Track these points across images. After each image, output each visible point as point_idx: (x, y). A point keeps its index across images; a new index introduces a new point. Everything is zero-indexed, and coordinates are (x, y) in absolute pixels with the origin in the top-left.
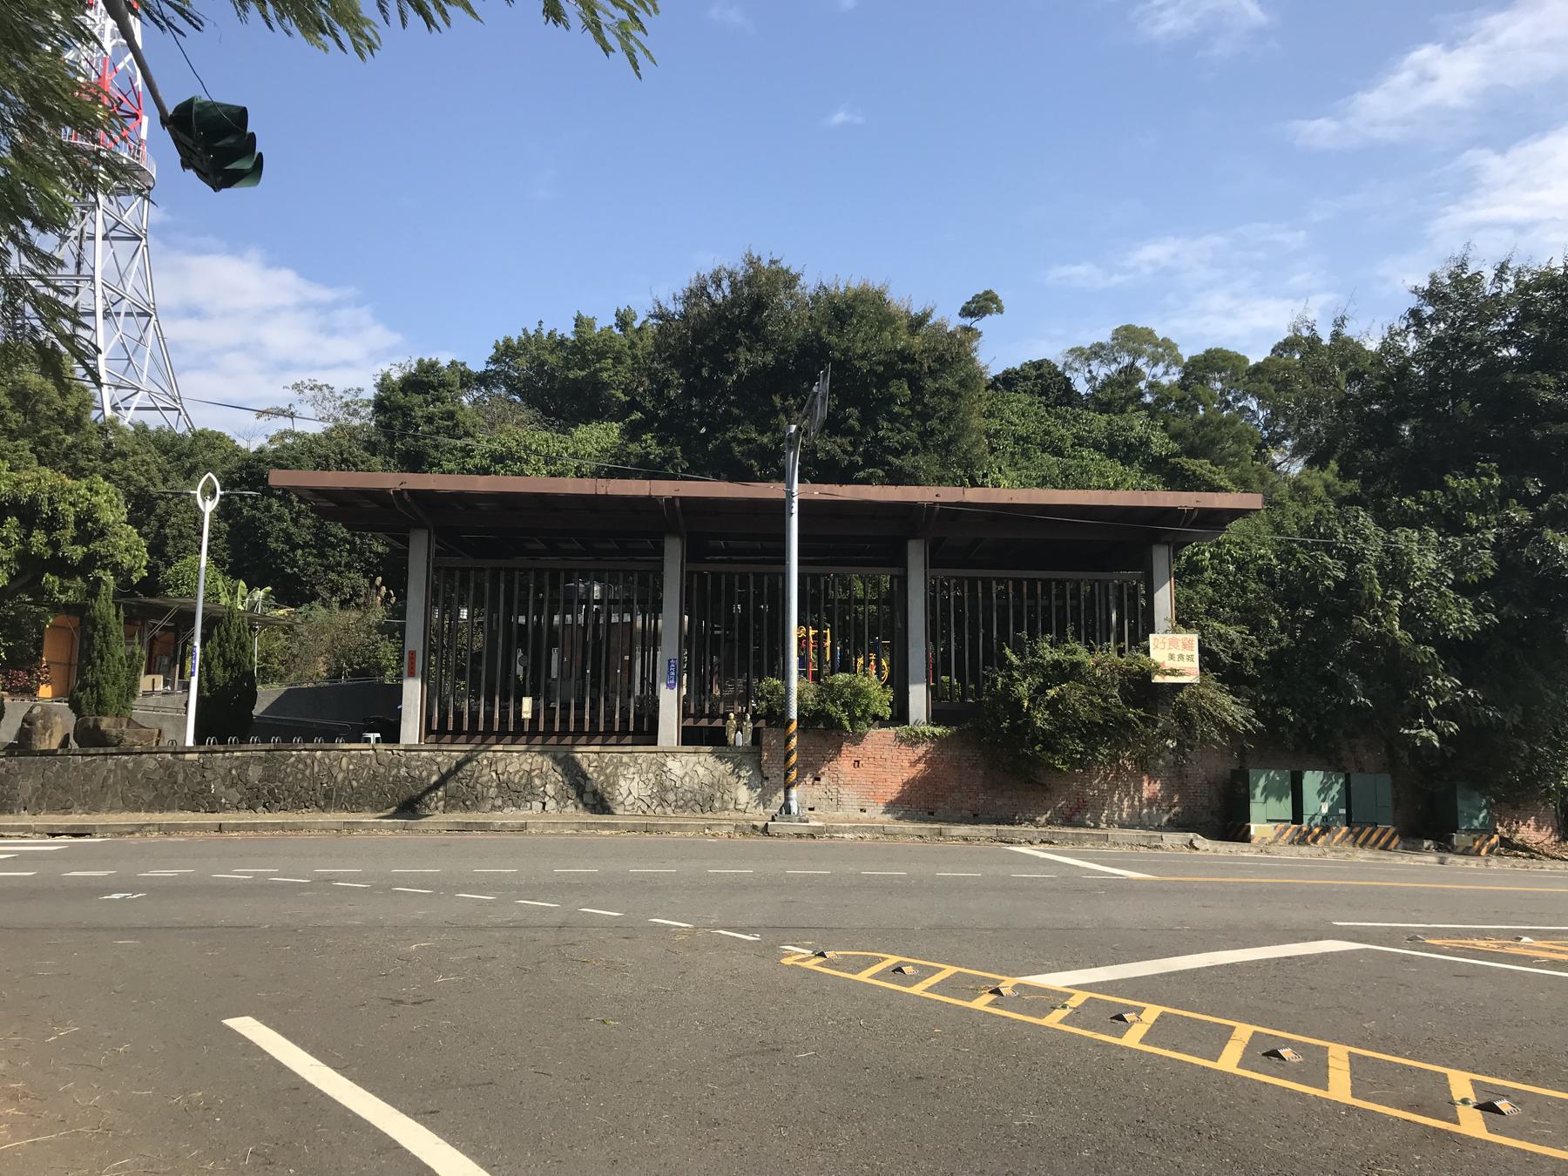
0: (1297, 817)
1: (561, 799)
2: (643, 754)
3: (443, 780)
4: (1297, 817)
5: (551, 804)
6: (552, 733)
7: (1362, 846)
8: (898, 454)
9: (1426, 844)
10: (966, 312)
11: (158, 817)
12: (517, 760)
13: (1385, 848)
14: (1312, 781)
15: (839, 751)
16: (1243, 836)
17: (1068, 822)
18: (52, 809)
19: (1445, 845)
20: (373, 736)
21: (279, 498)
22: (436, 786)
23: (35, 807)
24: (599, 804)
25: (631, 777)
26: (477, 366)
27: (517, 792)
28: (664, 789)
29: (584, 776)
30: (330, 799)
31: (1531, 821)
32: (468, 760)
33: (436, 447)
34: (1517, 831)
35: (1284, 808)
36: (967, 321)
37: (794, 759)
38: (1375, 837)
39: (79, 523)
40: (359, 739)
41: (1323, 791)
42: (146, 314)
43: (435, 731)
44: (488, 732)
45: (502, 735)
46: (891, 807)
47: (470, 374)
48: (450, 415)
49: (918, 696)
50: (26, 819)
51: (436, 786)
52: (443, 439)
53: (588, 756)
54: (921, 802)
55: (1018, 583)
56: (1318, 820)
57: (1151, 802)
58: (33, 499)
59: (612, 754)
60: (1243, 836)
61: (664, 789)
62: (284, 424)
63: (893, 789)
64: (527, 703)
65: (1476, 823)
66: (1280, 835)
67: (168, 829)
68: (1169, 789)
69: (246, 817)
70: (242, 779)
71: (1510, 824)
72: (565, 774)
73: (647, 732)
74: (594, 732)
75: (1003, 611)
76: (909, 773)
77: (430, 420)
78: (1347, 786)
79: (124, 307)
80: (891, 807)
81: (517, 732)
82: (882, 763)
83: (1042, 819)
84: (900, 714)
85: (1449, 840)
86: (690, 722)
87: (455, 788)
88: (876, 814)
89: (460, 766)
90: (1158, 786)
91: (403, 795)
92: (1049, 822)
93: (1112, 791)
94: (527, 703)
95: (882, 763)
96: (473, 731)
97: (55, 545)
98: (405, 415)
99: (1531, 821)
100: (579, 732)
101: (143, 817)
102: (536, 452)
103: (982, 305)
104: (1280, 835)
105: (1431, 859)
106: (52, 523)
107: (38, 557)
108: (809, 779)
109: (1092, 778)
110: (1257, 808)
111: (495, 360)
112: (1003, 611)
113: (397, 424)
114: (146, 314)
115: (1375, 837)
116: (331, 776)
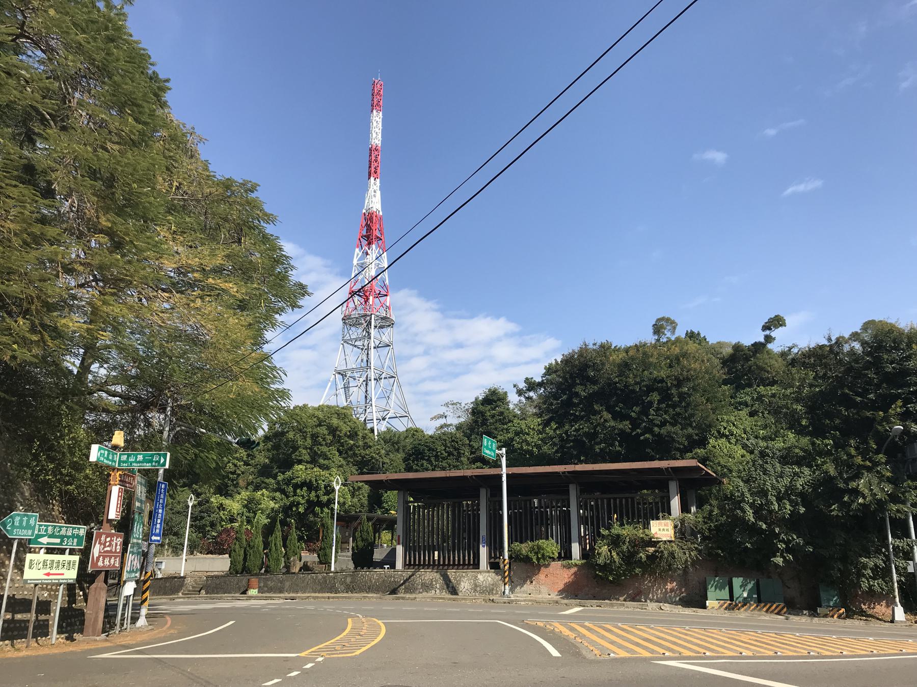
0: (731, 598)
1: (441, 589)
2: (471, 573)
3: (405, 582)
4: (731, 598)
5: (438, 591)
6: (441, 567)
7: (767, 611)
8: (660, 427)
9: (805, 612)
10: (766, 327)
11: (313, 595)
12: (429, 575)
13: (778, 613)
14: (737, 582)
15: (539, 570)
16: (704, 607)
17: (633, 600)
18: (293, 592)
19: (814, 614)
20: (386, 567)
21: (427, 460)
22: (402, 584)
23: (289, 591)
24: (454, 591)
25: (465, 581)
26: (538, 379)
27: (427, 587)
28: (476, 586)
29: (450, 581)
30: (370, 589)
31: (884, 603)
32: (413, 575)
33: (496, 429)
34: (874, 608)
35: (725, 593)
36: (767, 332)
37: (507, 574)
38: (774, 607)
39: (326, 487)
40: (383, 568)
41: (743, 586)
42: (393, 377)
43: (407, 565)
44: (419, 565)
45: (429, 566)
46: (561, 592)
47: (534, 383)
48: (502, 413)
49: (576, 549)
50: (287, 595)
51: (402, 584)
52: (498, 425)
53: (451, 573)
54: (573, 591)
55: (627, 499)
56: (741, 599)
57: (672, 590)
58: (310, 480)
59: (460, 573)
60: (704, 607)
61: (476, 586)
62: (442, 421)
63: (561, 586)
64: (436, 553)
65: (831, 604)
66: (721, 606)
67: (314, 598)
68: (680, 586)
69: (345, 595)
70: (345, 582)
71: (869, 605)
72: (444, 580)
73: (476, 565)
74: (454, 564)
75: (536, 519)
76: (567, 580)
77: (493, 416)
78: (757, 585)
79: (383, 376)
80: (561, 592)
81: (432, 565)
82: (557, 575)
83: (622, 599)
84: (566, 554)
85: (816, 611)
86: (492, 560)
87: (408, 585)
88: (554, 596)
89: (410, 577)
90: (675, 584)
91: (392, 588)
92: (625, 600)
93: (653, 586)
94: (436, 553)
95: (557, 575)
96: (415, 565)
97: (318, 496)
98: (483, 416)
99: (884, 603)
100: (449, 565)
101: (317, 595)
102: (533, 429)
103: (776, 322)
104: (721, 606)
105: (862, 623)
106: (317, 489)
107: (313, 501)
108: (528, 582)
109: (644, 581)
110: (711, 592)
111: (545, 375)
112: (536, 519)
113: (480, 420)
114: (393, 377)
115: (774, 607)
116: (371, 581)
